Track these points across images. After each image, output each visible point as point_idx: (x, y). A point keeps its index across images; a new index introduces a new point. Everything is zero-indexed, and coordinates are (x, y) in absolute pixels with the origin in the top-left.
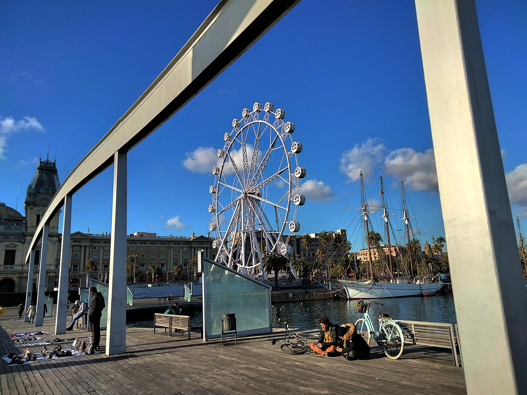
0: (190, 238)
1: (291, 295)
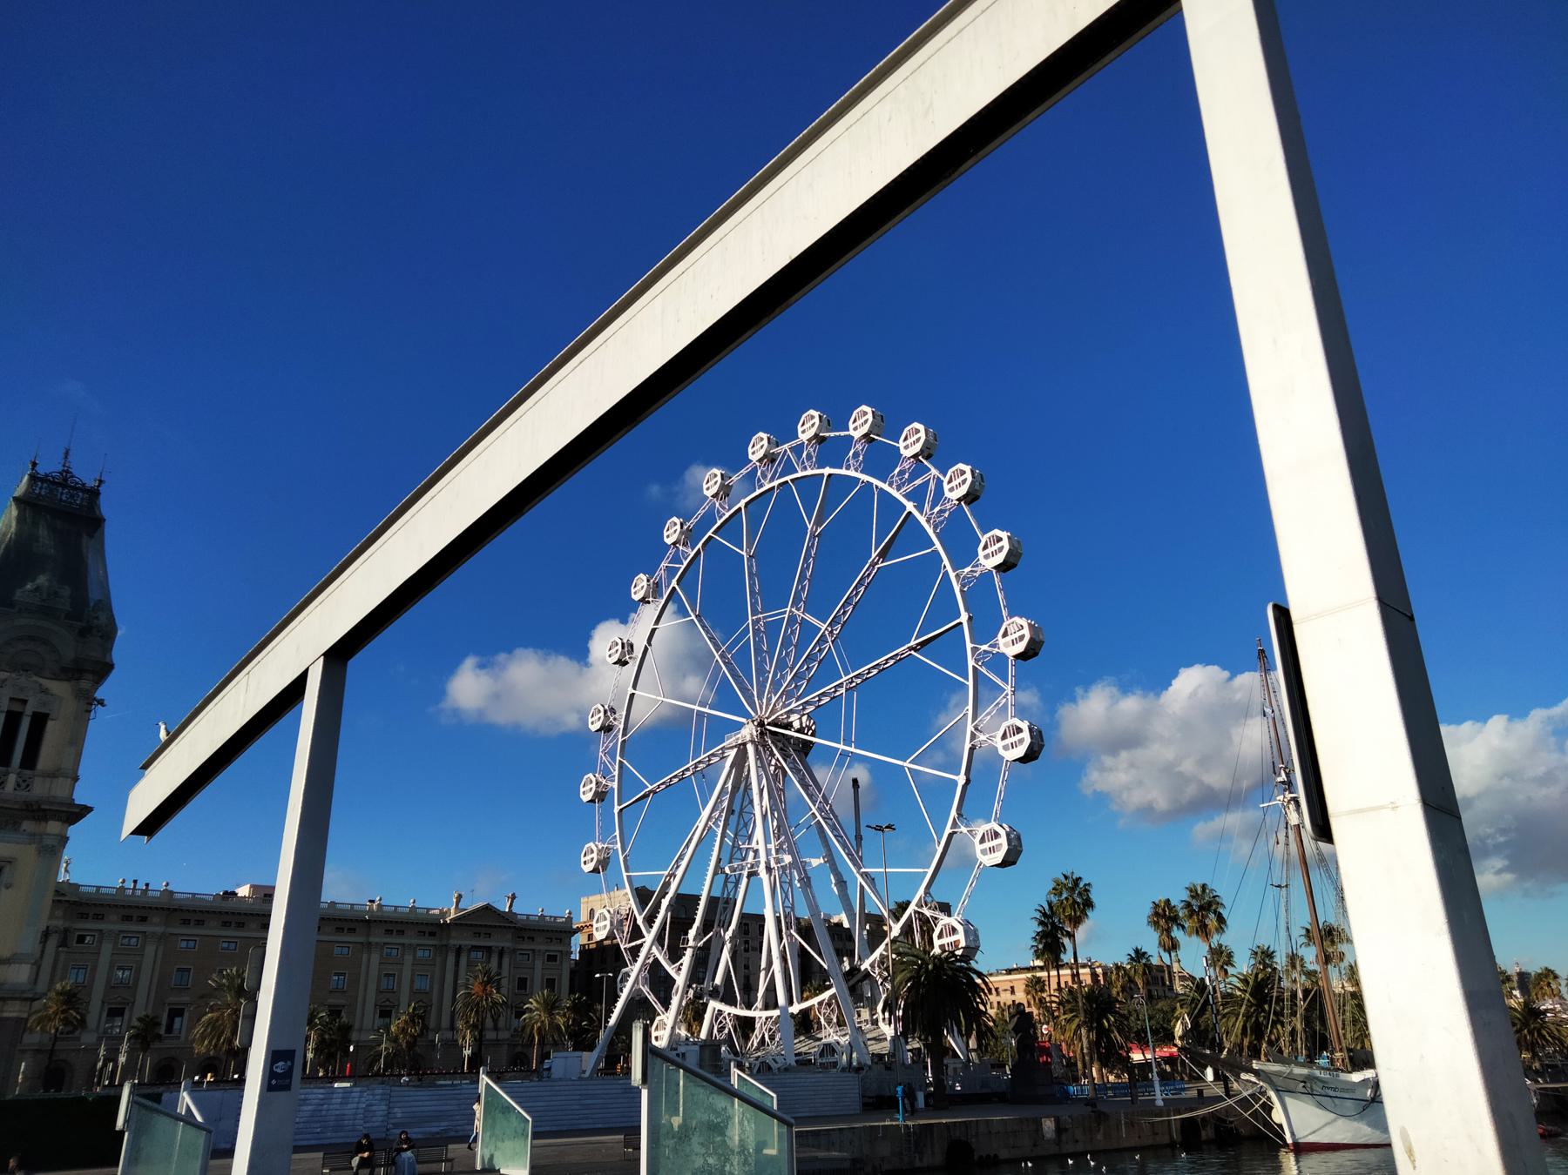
0: (443, 914)
1: (1049, 1125)
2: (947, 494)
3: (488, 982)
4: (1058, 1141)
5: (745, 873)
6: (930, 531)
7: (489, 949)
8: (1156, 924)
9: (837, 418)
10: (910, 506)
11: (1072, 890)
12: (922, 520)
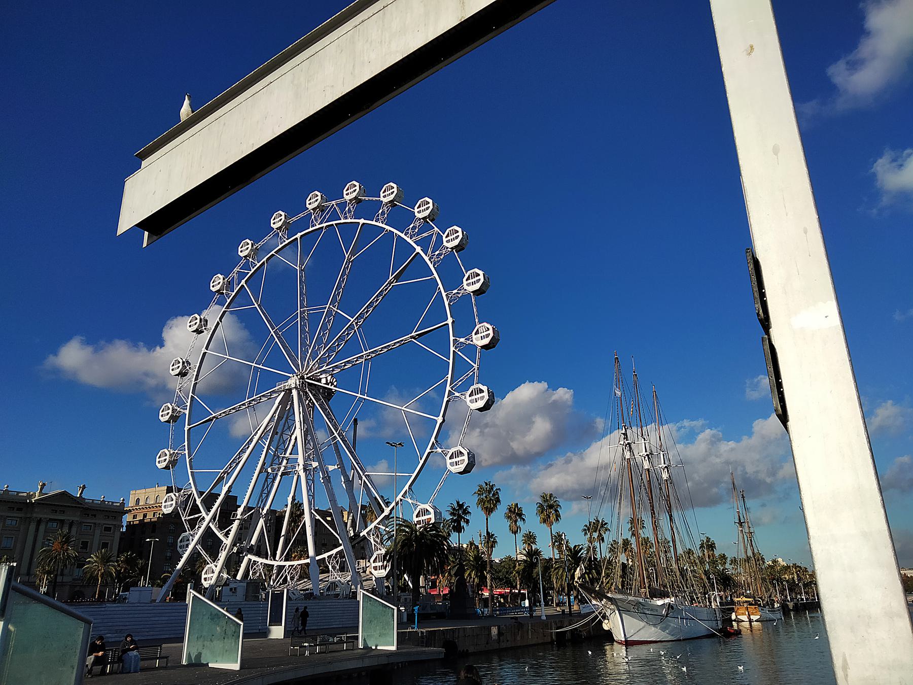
0: (30, 496)
2: (445, 244)
3: (65, 542)
4: (499, 641)
5: (280, 474)
6: (431, 266)
7: (62, 522)
8: (509, 517)
9: (372, 187)
10: (418, 249)
11: (489, 492)
12: (426, 259)
